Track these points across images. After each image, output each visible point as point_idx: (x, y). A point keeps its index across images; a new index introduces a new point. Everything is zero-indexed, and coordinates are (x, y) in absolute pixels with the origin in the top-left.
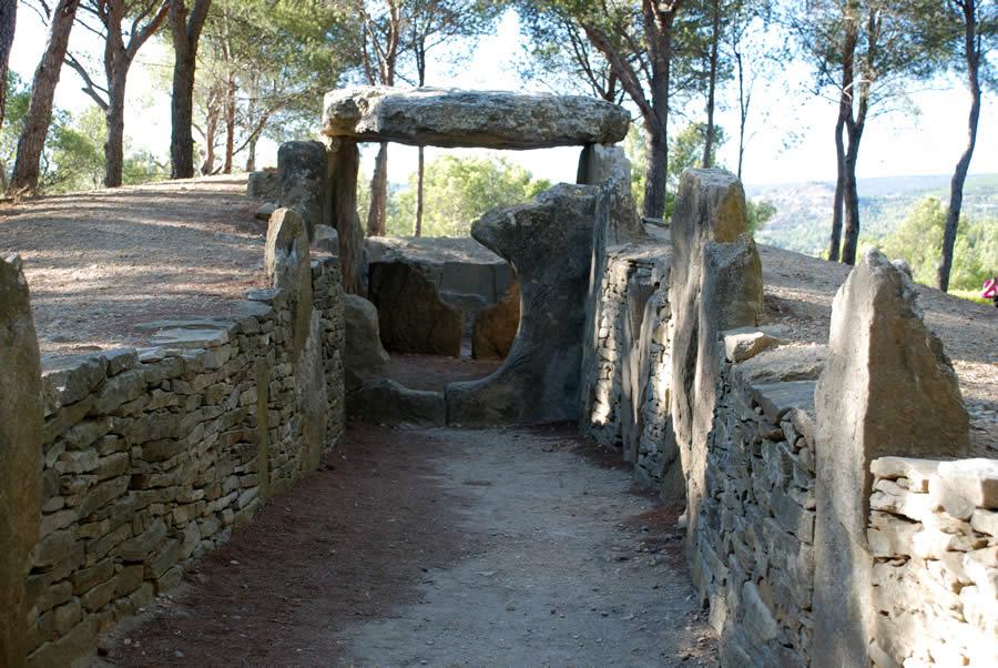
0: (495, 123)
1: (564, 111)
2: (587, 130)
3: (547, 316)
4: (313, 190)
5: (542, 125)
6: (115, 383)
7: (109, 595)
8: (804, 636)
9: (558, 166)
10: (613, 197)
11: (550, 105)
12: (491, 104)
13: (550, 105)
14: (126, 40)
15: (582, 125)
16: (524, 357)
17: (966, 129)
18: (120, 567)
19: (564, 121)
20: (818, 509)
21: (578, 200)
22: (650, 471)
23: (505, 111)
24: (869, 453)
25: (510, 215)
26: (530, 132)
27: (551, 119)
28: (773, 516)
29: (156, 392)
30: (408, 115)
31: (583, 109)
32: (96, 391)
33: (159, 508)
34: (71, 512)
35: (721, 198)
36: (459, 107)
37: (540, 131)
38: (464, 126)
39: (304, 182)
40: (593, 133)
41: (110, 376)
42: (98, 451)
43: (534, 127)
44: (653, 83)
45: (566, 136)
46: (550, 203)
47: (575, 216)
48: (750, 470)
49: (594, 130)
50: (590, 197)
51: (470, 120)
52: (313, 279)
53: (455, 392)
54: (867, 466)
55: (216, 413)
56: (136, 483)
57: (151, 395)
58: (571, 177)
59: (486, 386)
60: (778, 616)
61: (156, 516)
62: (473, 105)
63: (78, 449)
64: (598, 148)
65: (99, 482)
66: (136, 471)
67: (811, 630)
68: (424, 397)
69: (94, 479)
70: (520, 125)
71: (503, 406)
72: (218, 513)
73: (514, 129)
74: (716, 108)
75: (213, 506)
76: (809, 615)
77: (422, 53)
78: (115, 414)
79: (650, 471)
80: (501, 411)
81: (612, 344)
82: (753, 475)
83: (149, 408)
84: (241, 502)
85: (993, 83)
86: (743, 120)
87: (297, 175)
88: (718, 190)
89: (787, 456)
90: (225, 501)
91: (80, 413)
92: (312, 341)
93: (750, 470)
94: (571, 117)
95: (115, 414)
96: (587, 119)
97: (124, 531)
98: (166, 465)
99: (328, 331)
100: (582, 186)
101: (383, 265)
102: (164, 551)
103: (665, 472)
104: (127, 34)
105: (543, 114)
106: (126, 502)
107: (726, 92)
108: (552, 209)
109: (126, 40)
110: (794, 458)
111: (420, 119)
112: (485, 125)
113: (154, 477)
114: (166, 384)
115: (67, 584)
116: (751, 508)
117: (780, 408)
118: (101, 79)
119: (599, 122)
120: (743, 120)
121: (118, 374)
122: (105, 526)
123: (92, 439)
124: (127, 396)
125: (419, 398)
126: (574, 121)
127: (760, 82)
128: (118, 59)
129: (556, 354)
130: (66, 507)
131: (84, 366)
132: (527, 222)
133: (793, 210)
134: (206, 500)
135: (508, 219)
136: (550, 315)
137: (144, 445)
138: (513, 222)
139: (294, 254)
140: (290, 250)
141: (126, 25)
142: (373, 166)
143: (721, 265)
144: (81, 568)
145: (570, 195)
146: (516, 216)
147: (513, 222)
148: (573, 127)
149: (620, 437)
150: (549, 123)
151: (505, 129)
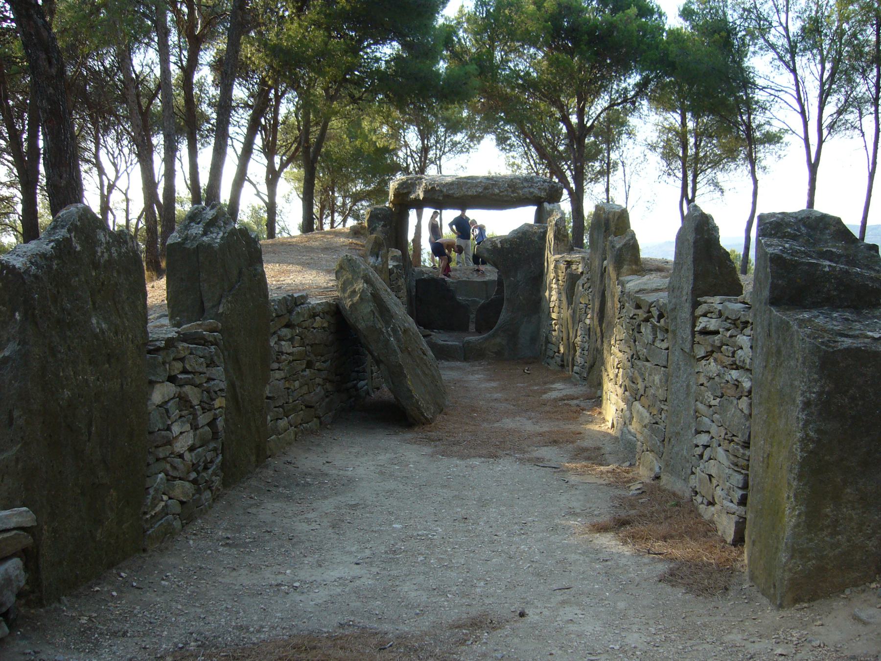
1: (526, 184)
2: (539, 195)
5: (513, 192)
6: (299, 309)
8: (663, 414)
9: (525, 215)
11: (518, 181)
14: (277, 167)
18: (304, 408)
19: (526, 190)
20: (670, 348)
21: (535, 232)
23: (493, 184)
25: (497, 242)
26: (507, 196)
29: (318, 318)
32: (290, 312)
34: (282, 372)
35: (616, 217)
36: (467, 183)
38: (470, 193)
40: (542, 196)
41: (297, 306)
42: (292, 344)
43: (509, 193)
44: (574, 178)
45: (527, 198)
47: (534, 241)
49: (543, 194)
50: (542, 230)
52: (390, 275)
53: (469, 342)
57: (315, 320)
58: (532, 221)
60: (650, 411)
64: (546, 205)
65: (293, 360)
66: (309, 359)
67: (667, 410)
68: (452, 345)
69: (291, 358)
70: (502, 192)
74: (611, 189)
76: (666, 403)
77: (440, 166)
78: (299, 325)
81: (556, 309)
82: (637, 343)
86: (627, 198)
88: (615, 213)
91: (284, 321)
93: (635, 341)
94: (530, 187)
95: (299, 325)
97: (305, 388)
100: (538, 224)
101: (424, 280)
106: (305, 373)
107: (616, 178)
109: (277, 167)
110: (658, 324)
112: (482, 192)
113: (318, 364)
114: (321, 315)
115: (281, 409)
118: (264, 189)
119: (546, 190)
120: (627, 198)
121: (300, 305)
122: (297, 384)
123: (289, 336)
124: (304, 317)
126: (532, 190)
127: (635, 177)
128: (272, 177)
130: (279, 369)
131: (284, 297)
132: (507, 246)
135: (496, 244)
137: (312, 346)
138: (499, 246)
139: (380, 259)
140: (378, 257)
141: (277, 160)
142: (414, 231)
143: (618, 247)
144: (287, 403)
147: (499, 246)
148: (531, 193)
149: (562, 361)
151: (494, 195)
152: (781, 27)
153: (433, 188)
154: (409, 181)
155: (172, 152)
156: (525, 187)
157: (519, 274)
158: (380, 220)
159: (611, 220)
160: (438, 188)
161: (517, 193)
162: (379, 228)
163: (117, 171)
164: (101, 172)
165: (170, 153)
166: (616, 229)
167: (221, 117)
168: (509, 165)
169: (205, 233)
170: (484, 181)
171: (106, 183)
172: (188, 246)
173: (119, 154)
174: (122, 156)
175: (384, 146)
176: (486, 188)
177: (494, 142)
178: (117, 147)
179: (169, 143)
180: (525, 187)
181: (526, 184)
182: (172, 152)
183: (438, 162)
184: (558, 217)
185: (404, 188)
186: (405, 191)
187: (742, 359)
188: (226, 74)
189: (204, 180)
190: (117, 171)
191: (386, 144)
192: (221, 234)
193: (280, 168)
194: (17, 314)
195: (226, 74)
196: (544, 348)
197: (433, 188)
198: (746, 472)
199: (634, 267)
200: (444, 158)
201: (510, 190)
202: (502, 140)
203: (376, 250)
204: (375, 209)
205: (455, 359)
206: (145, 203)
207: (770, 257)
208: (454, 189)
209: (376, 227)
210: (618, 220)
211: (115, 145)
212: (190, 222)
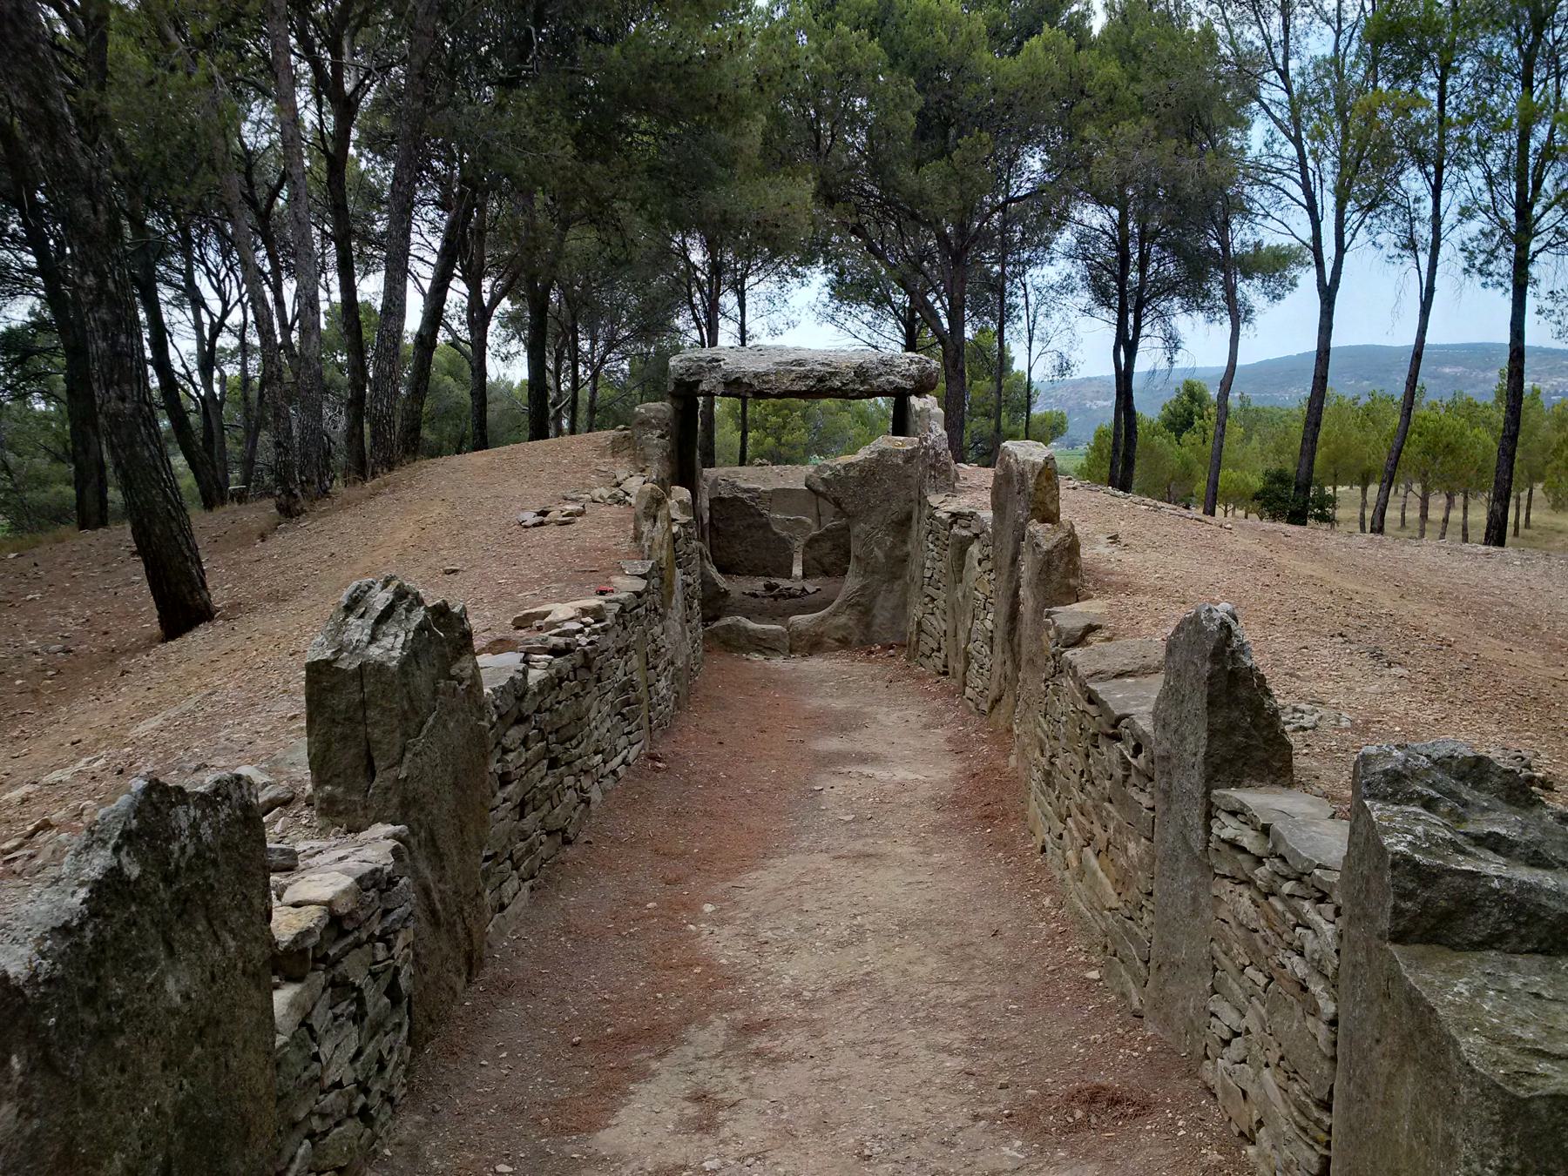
5: (862, 383)
7: (537, 863)
10: (932, 452)
12: (819, 367)
14: (486, 297)
22: (977, 705)
24: (1210, 782)
28: (1111, 802)
30: (746, 380)
31: (899, 366)
33: (569, 780)
35: (1037, 472)
44: (949, 316)
48: (1088, 756)
49: (909, 385)
54: (1207, 794)
55: (609, 687)
56: (554, 763)
59: (823, 619)
61: (569, 787)
63: (512, 751)
64: (913, 400)
70: (844, 384)
71: (839, 636)
72: (614, 772)
73: (839, 388)
75: (611, 766)
79: (977, 705)
80: (838, 640)
83: (560, 698)
84: (631, 758)
88: (1034, 464)
89: (1125, 758)
90: (619, 759)
92: (678, 599)
93: (1088, 756)
98: (574, 742)
99: (689, 585)
102: (576, 816)
103: (992, 709)
106: (546, 783)
109: (486, 297)
116: (1089, 787)
117: (1117, 713)
125: (765, 632)
133: (1070, 403)
134: (605, 762)
139: (658, 524)
141: (487, 284)
146: (844, 468)
148: (891, 383)
152: (1274, 73)
163: (225, 303)
164: (198, 303)
169: (373, 639)
171: (205, 318)
172: (343, 665)
173: (227, 275)
174: (233, 277)
176: (821, 380)
178: (224, 263)
180: (881, 374)
187: (1317, 956)
190: (225, 303)
192: (401, 639)
193: (490, 302)
194: (14, 1059)
196: (915, 639)
198: (1325, 1152)
201: (858, 380)
207: (1393, 860)
211: (219, 259)
212: (347, 617)
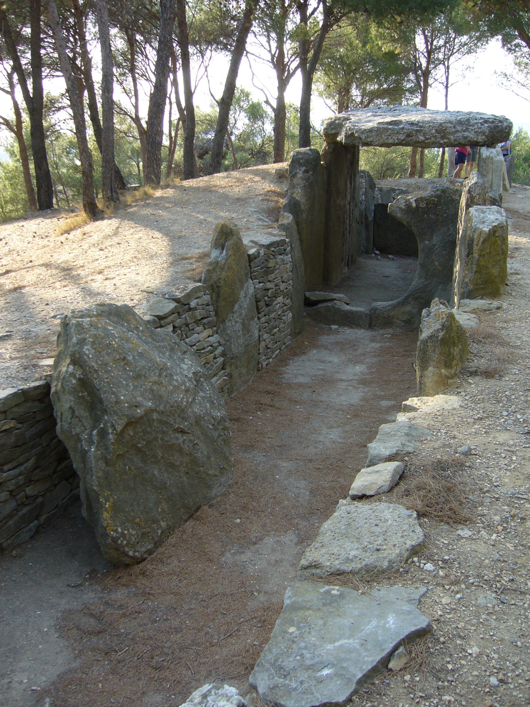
0: (410, 139)
1: (459, 128)
2: (475, 139)
3: (435, 264)
4: (307, 180)
5: (443, 138)
11: (449, 125)
13: (449, 125)
15: (471, 136)
16: (419, 289)
17: (445, 98)
19: (459, 134)
25: (411, 200)
27: (450, 133)
36: (388, 129)
37: (442, 142)
39: (301, 175)
43: (438, 140)
46: (439, 193)
51: (394, 137)
62: (396, 127)
68: (356, 312)
70: (427, 139)
73: (423, 142)
77: (448, 67)
80: (404, 321)
85: (7, 123)
87: (298, 171)
94: (464, 131)
96: (476, 132)
104: (98, 83)
105: (444, 131)
108: (438, 197)
111: (364, 138)
126: (466, 134)
129: (440, 287)
132: (423, 205)
135: (410, 203)
136: (436, 263)
138: (414, 205)
139: (224, 252)
140: (223, 249)
145: (452, 187)
147: (414, 205)
148: (465, 138)
150: (448, 136)
153: (352, 134)
154: (337, 122)
155: (108, 93)
156: (458, 131)
157: (435, 238)
158: (301, 165)
159: (475, 243)
160: (356, 135)
161: (448, 138)
162: (300, 175)
165: (107, 94)
166: (480, 255)
167: (161, 54)
168: (516, 64)
170: (408, 127)
175: (389, 51)
177: (500, 43)
179: (106, 85)
180: (458, 131)
181: (459, 128)
182: (108, 93)
183: (446, 63)
184: (473, 182)
185: (332, 129)
186: (334, 132)
188: (165, 7)
189: (183, 105)
191: (392, 48)
195: (165, 7)
197: (352, 134)
199: (443, 371)
200: (452, 59)
202: (506, 41)
203: (221, 241)
204: (298, 153)
205: (358, 326)
206: (224, 93)
208: (372, 136)
209: (296, 173)
210: (483, 242)
